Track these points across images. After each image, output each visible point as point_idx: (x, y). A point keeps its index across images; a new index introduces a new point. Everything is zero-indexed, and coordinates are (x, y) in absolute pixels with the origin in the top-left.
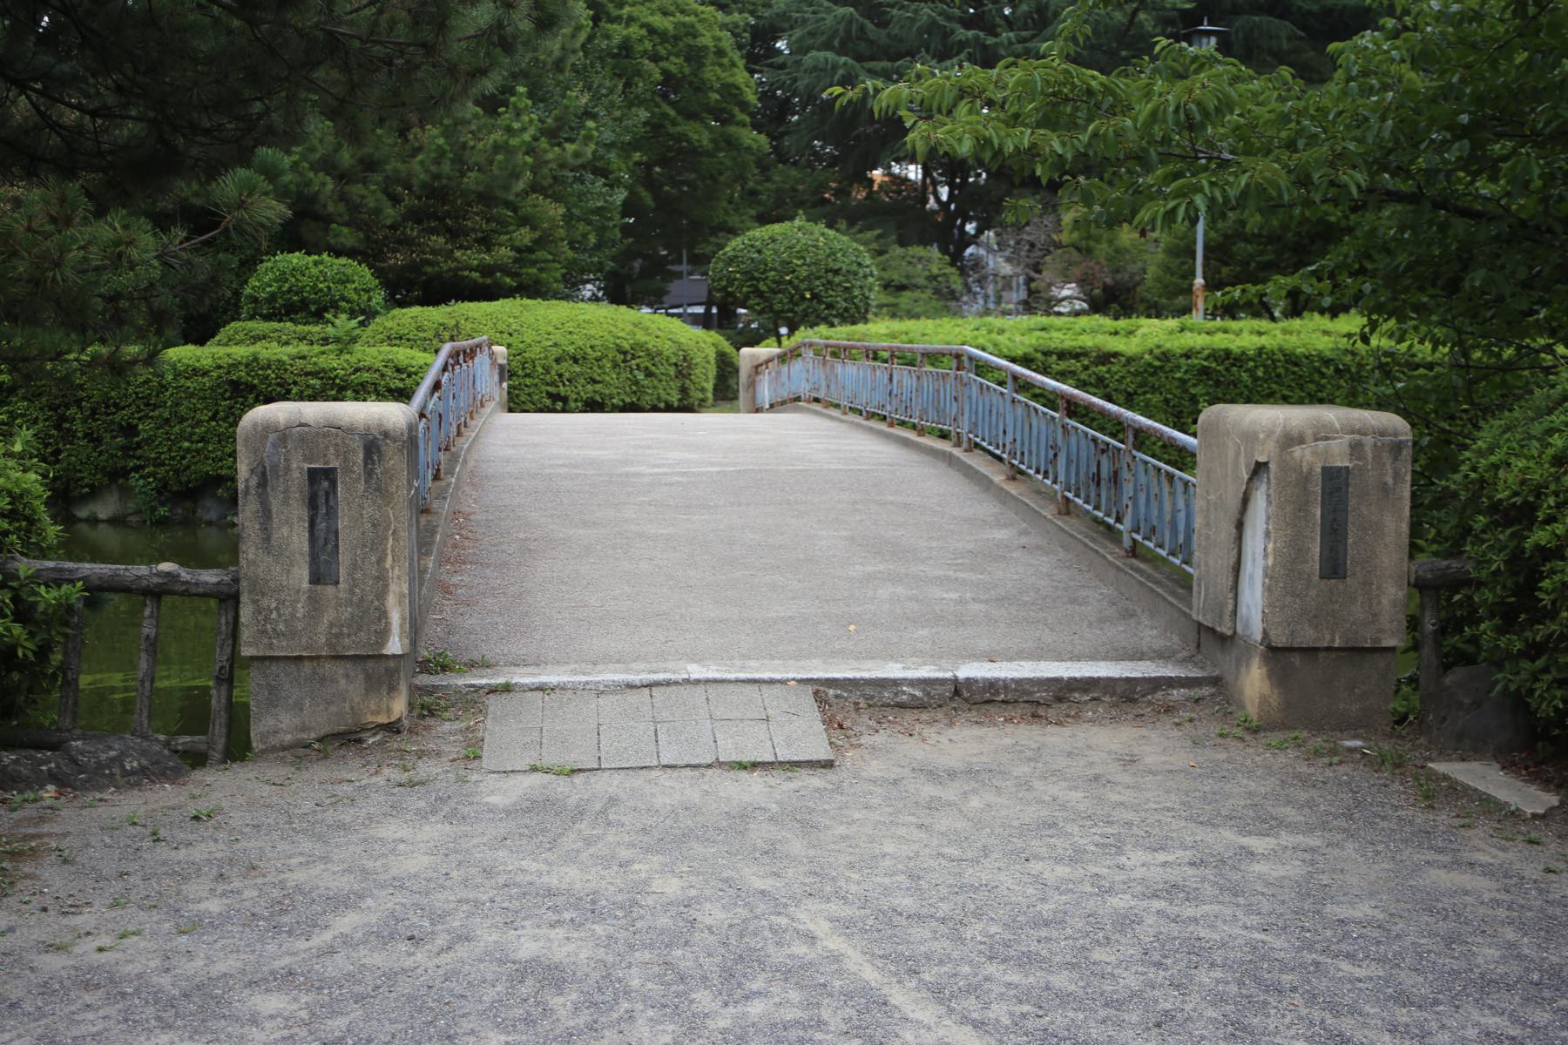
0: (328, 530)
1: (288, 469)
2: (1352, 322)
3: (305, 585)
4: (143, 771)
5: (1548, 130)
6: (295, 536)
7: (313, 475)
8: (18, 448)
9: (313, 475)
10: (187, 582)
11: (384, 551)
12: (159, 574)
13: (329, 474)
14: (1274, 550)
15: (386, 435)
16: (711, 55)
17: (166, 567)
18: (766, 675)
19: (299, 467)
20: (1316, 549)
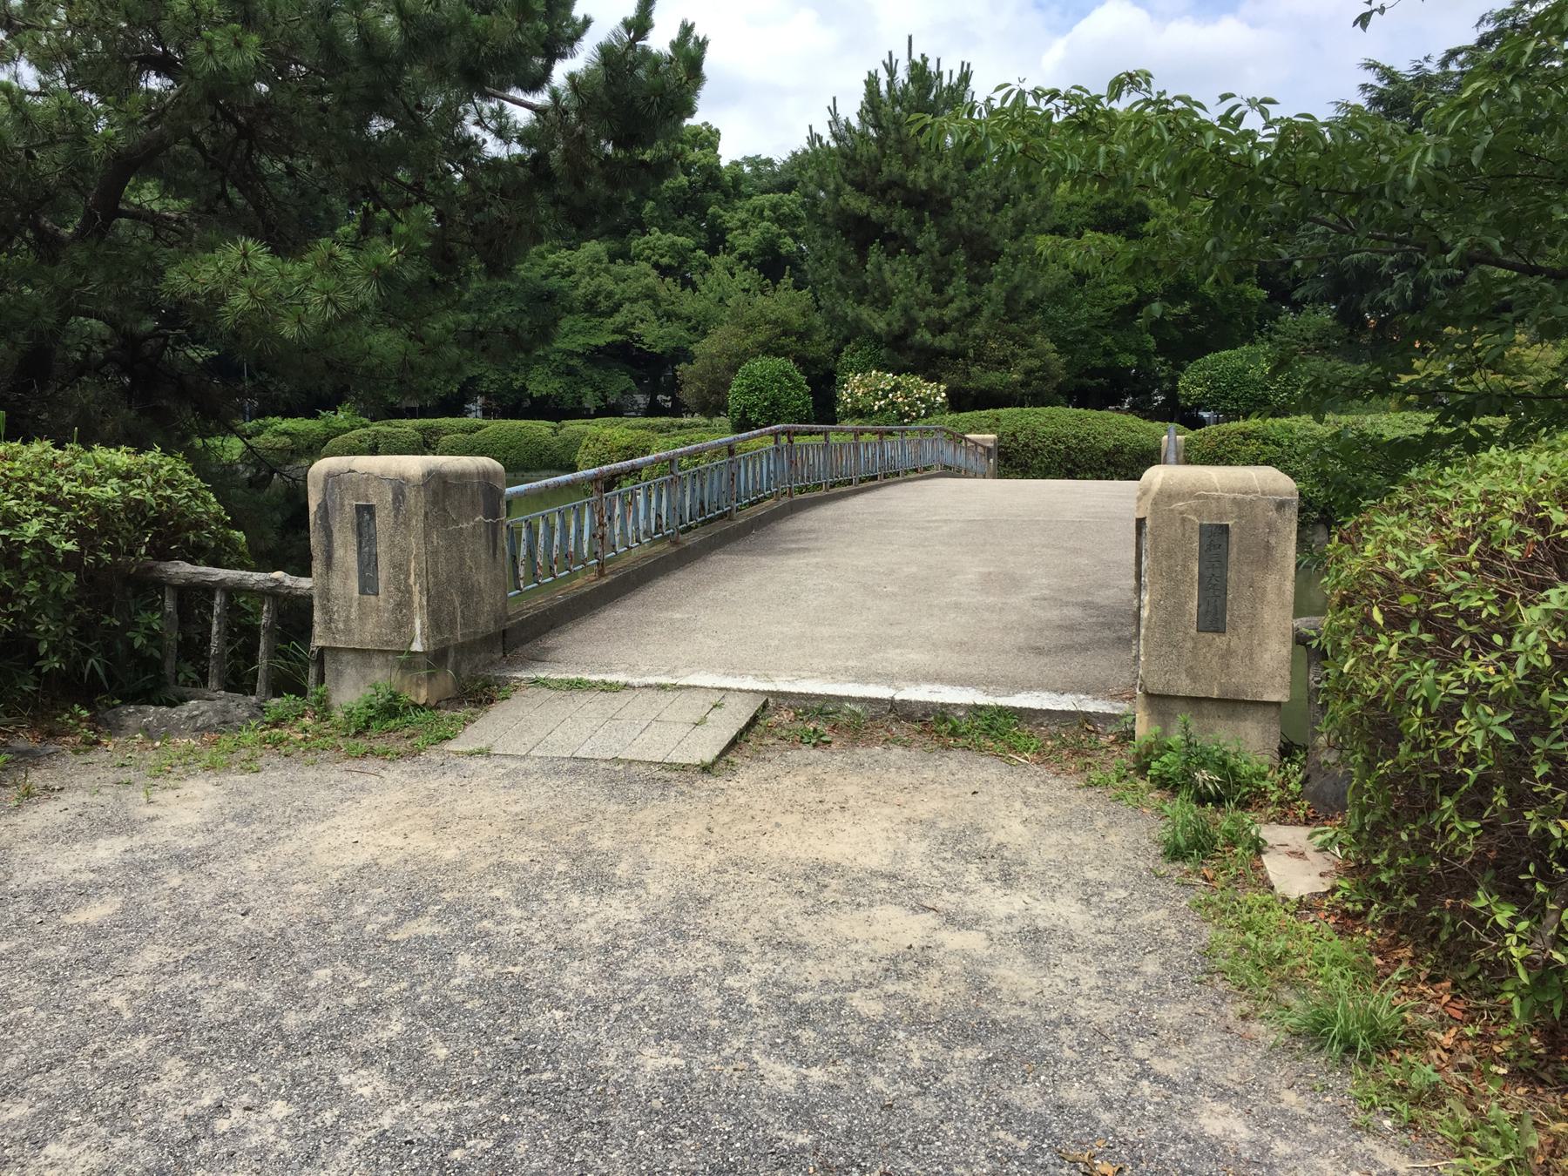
0: (370, 553)
1: (342, 505)
2: (1365, 366)
3: (356, 594)
4: (391, 709)
5: (1007, 105)
6: (346, 553)
7: (360, 509)
8: (1126, 406)
9: (360, 509)
10: (289, 587)
11: (408, 570)
12: (271, 580)
13: (370, 509)
14: (1150, 601)
15: (408, 481)
16: (609, 193)
17: (278, 574)
18: (1144, 566)
19: (350, 503)
20: (1193, 605)
